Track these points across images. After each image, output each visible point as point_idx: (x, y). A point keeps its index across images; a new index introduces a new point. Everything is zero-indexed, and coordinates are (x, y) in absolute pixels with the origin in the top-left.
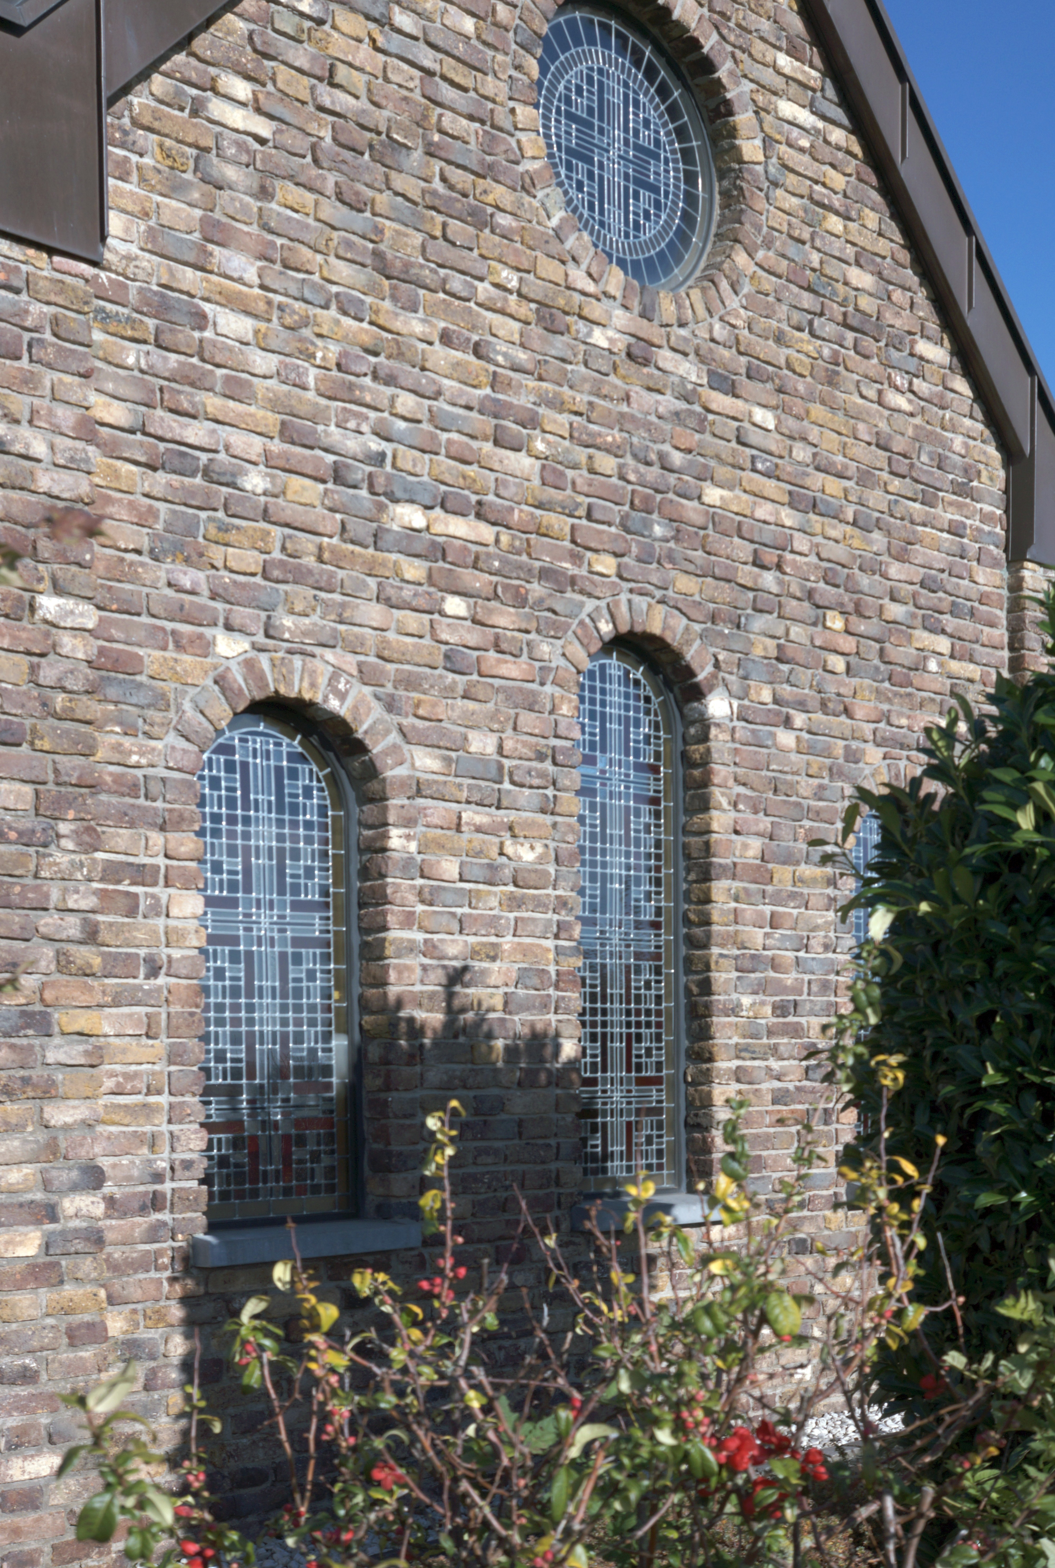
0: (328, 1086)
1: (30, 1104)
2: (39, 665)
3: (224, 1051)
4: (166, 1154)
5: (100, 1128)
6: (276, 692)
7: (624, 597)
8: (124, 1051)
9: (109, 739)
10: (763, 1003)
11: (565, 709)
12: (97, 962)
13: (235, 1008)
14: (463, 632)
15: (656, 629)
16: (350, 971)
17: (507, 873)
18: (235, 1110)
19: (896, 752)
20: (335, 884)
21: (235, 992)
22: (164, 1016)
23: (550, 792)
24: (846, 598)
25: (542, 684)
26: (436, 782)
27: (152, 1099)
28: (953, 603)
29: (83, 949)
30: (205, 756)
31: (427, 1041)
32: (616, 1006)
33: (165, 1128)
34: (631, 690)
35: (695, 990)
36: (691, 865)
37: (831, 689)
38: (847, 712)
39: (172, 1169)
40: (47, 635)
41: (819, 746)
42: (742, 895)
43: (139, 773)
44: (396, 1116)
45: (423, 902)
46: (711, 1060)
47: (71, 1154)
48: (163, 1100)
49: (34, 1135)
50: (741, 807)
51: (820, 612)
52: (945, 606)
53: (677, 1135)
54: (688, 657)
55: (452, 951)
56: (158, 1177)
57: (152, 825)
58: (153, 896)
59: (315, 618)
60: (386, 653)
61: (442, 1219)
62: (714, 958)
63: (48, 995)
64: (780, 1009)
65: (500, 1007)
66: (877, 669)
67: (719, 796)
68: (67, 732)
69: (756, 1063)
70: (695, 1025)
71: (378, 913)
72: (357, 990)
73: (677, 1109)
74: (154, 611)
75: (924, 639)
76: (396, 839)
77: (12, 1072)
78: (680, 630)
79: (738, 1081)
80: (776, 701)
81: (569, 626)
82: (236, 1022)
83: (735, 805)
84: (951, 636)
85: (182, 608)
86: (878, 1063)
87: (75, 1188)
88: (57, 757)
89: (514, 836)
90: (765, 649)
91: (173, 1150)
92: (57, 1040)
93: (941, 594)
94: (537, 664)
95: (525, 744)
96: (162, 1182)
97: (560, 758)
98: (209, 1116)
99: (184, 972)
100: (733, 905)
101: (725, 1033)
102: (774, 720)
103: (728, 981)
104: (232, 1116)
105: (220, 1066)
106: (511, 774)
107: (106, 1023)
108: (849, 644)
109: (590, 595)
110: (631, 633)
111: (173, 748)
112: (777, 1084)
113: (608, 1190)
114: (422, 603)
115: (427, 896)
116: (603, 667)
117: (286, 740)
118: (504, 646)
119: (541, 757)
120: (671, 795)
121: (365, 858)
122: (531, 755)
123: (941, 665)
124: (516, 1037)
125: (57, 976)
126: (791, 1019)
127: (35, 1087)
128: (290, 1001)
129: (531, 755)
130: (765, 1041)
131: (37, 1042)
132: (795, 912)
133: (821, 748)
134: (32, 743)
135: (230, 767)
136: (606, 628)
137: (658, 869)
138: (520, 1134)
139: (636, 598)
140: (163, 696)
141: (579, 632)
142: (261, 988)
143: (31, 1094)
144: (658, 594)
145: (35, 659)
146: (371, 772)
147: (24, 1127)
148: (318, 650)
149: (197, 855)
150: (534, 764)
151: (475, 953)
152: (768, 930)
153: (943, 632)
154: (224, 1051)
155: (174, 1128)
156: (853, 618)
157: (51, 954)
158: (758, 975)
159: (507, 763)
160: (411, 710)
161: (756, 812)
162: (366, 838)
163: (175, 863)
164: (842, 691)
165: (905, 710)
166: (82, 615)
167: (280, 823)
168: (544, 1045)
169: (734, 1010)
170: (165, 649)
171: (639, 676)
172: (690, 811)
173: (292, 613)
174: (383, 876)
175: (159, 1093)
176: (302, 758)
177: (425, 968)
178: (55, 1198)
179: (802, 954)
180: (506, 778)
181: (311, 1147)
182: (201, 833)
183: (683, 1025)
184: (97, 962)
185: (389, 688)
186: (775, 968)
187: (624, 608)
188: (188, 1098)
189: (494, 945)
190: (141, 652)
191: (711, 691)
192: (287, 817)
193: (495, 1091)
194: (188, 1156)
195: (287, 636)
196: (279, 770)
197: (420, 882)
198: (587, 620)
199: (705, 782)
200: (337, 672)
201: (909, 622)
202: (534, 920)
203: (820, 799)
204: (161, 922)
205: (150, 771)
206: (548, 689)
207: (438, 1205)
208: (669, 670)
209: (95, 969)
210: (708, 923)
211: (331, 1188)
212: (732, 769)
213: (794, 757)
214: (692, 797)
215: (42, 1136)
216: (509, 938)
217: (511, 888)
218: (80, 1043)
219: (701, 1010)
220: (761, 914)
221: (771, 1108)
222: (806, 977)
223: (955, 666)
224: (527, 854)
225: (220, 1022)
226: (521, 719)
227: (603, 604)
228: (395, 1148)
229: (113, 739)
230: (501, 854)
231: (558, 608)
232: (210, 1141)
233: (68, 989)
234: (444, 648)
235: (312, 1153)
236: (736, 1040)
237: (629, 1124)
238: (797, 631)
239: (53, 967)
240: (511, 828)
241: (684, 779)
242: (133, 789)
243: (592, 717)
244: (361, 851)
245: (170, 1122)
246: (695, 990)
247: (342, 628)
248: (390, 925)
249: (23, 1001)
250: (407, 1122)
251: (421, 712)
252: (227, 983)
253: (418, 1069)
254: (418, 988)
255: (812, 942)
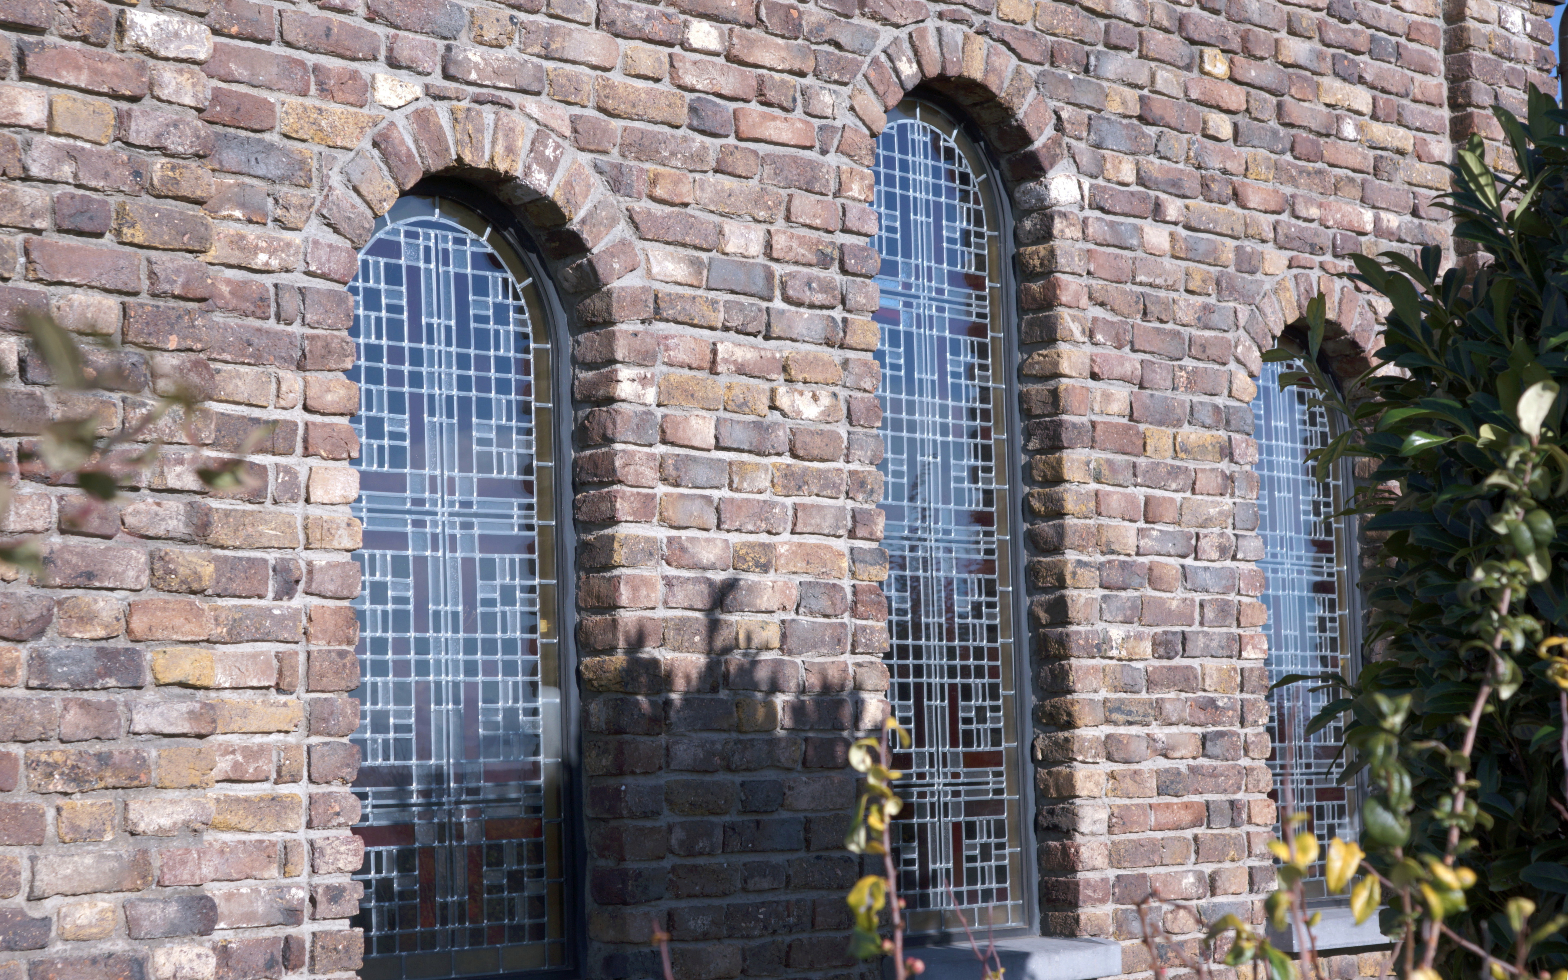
0: (535, 769)
1: (109, 797)
2: (129, 114)
3: (385, 714)
4: (303, 879)
5: (209, 836)
6: (459, 159)
7: (931, 24)
8: (245, 713)
9: (227, 229)
10: (1139, 637)
11: (856, 190)
12: (208, 570)
13: (401, 646)
14: (715, 74)
15: (976, 72)
16: (562, 586)
17: (782, 436)
18: (404, 806)
19: (1305, 257)
20: (540, 456)
21: (400, 620)
22: (302, 657)
23: (838, 314)
24: (1230, 29)
25: (824, 152)
26: (681, 297)
27: (284, 789)
28: (1373, 39)
29: (188, 550)
30: (360, 256)
31: (675, 696)
32: (934, 642)
33: (303, 835)
34: (942, 164)
35: (1044, 617)
36: (1030, 428)
37: (1215, 162)
38: (1236, 196)
39: (313, 901)
40: (142, 68)
41: (1202, 248)
42: (1106, 472)
43: (268, 281)
44: (633, 816)
45: (664, 480)
46: (1070, 725)
47: (168, 879)
48: (301, 790)
49: (115, 848)
50: (1099, 337)
51: (1195, 49)
52: (1362, 43)
53: (1023, 843)
54: (1020, 115)
55: (707, 555)
56: (292, 915)
57: (286, 360)
58: (288, 470)
59: (511, 50)
60: (610, 104)
61: (886, 929)
62: (1069, 568)
63: (138, 624)
64: (1164, 647)
65: (776, 643)
66: (1275, 133)
67: (1069, 321)
68: (168, 216)
69: (1134, 730)
70: (1045, 670)
71: (602, 498)
72: (572, 618)
73: (1021, 805)
74: (289, 37)
75: (1336, 90)
76: (627, 384)
77: (83, 746)
78: (1008, 74)
79: (1110, 758)
80: (1141, 181)
81: (859, 65)
82: (402, 668)
83: (1091, 336)
84: (1373, 87)
85: (328, 32)
86: (1550, 650)
87: (173, 933)
88: (153, 254)
89: (789, 381)
90: (1124, 103)
91: (314, 870)
92: (149, 695)
93: (1355, 25)
94: (817, 122)
95: (802, 241)
96: (299, 923)
97: (851, 263)
98: (364, 818)
99: (331, 588)
100: (1094, 486)
101: (1090, 684)
102: (1139, 208)
103: (1089, 602)
104: (398, 816)
105: (380, 737)
106: (784, 286)
107: (219, 667)
108: (1235, 97)
109: (885, 21)
110: (942, 78)
111: (316, 243)
112: (1163, 763)
113: (932, 932)
114: (658, 29)
115: (671, 471)
116: (902, 129)
117: (471, 235)
118: (771, 95)
119: (824, 262)
120: (1000, 322)
121: (581, 414)
122: (812, 258)
123: (1360, 128)
124: (803, 690)
125: (149, 594)
126: (1178, 661)
127: (117, 769)
128: (479, 635)
129: (812, 258)
130: (1144, 695)
131: (120, 697)
132: (1178, 496)
133: (1240, 231)
134: (118, 233)
135: (393, 275)
136: (908, 70)
137: (986, 433)
138: (808, 842)
139: (948, 27)
140: (302, 163)
141: (872, 75)
142: (437, 614)
143: (111, 781)
144: (978, 20)
145: (124, 105)
146: (591, 282)
147: (101, 833)
148: (516, 99)
149: (350, 406)
150: (815, 271)
151: (738, 560)
152: (1141, 524)
153: (1361, 80)
154: (385, 714)
155: (316, 835)
156: (1239, 59)
157: (143, 559)
158: (1131, 593)
159: (778, 269)
160: (644, 189)
161: (1119, 347)
162: (584, 383)
163: (317, 419)
164: (1229, 166)
165: (1314, 195)
166: (190, 39)
167: (463, 362)
168: (841, 702)
169: (1100, 648)
170: (304, 94)
171: (952, 143)
172: (1028, 346)
173: (480, 41)
174: (609, 440)
175: (294, 779)
176: (493, 263)
177: (669, 583)
178: (143, 949)
179: (1189, 561)
180: (778, 293)
181: (510, 865)
182: (353, 374)
183: (1028, 673)
184: (208, 570)
185: (614, 156)
186: (1153, 582)
187: (932, 40)
188: (336, 788)
189: (767, 548)
190: (272, 97)
191: (1052, 166)
192: (472, 351)
193: (771, 775)
194: (336, 880)
195: (473, 76)
196: (461, 279)
197: (660, 449)
198: (883, 58)
199: (1049, 301)
200: (544, 129)
201: (1314, 66)
202: (820, 508)
203: (1207, 327)
204: (298, 509)
205: (284, 278)
206: (832, 159)
207: (880, 904)
208: (993, 134)
209: (206, 583)
210: (1060, 514)
211: (538, 932)
212: (1085, 280)
213: (1168, 263)
214: (1031, 323)
215: (126, 849)
216: (786, 536)
217: (787, 459)
218: (182, 698)
219: (1054, 648)
220: (1131, 500)
221: (1155, 800)
222: (1198, 597)
223: (1380, 131)
224: (807, 407)
225: (380, 669)
226: (796, 202)
227: (903, 34)
228: (631, 865)
229: (232, 228)
230: (773, 407)
231: (842, 40)
232: (367, 855)
233: (167, 614)
234: (689, 96)
235: (511, 875)
236: (1103, 694)
237: (957, 826)
238: (1166, 78)
239: (145, 579)
240: (785, 369)
241: (1017, 299)
242: (259, 306)
243: (891, 205)
244: (576, 404)
245: (309, 825)
246: (1044, 617)
247: (549, 65)
248: (620, 516)
249: (101, 633)
250: (649, 824)
251: (659, 192)
252: (390, 607)
253: (663, 739)
254: (661, 613)
255: (1203, 543)
